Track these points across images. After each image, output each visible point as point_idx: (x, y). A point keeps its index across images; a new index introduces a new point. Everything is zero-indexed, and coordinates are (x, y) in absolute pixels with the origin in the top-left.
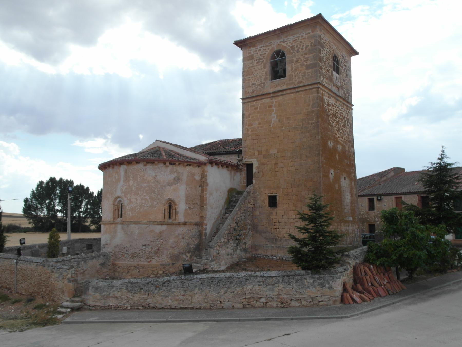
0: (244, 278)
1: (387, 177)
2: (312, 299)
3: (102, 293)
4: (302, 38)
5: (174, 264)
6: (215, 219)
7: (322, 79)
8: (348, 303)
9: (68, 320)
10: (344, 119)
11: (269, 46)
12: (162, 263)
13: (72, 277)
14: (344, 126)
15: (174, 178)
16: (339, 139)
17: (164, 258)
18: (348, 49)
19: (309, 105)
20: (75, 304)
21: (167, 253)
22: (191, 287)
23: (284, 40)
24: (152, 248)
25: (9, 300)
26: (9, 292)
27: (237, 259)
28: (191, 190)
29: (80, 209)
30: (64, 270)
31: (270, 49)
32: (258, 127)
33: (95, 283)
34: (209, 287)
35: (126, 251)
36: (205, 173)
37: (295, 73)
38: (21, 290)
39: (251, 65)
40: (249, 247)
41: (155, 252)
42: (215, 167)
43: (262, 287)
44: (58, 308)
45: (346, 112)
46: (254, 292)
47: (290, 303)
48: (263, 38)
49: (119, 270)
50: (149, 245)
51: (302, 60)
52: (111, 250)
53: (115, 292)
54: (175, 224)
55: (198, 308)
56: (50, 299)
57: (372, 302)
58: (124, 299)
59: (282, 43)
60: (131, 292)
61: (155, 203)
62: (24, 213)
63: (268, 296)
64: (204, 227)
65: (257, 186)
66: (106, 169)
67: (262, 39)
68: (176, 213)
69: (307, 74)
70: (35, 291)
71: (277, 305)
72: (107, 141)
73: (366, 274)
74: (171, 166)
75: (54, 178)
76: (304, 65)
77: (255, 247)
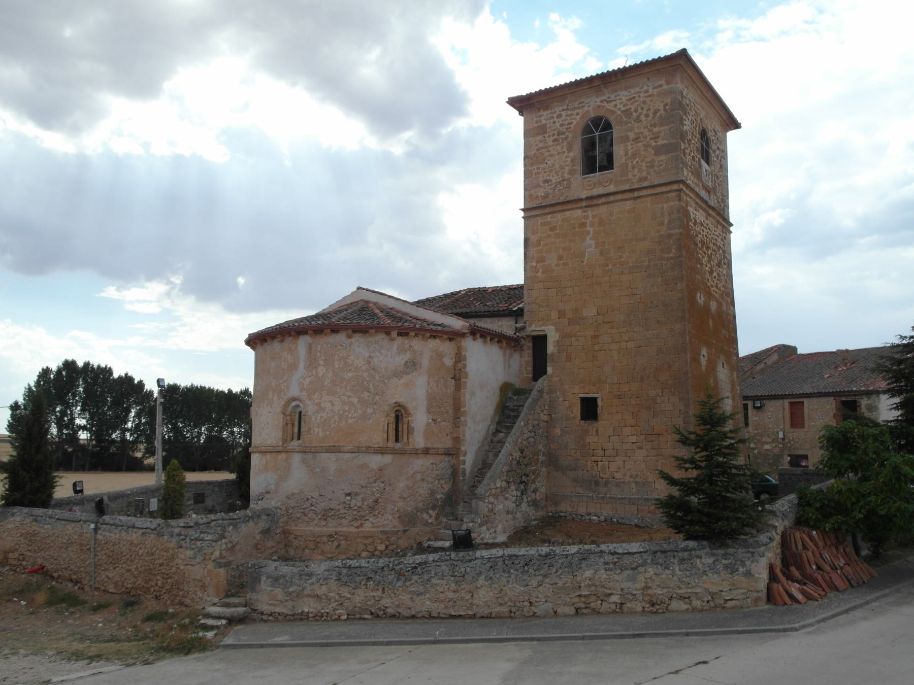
0: (577, 557)
1: (765, 363)
2: (713, 595)
3: (289, 588)
4: (646, 95)
5: (407, 530)
6: (479, 443)
7: (687, 175)
8: (782, 603)
9: (228, 640)
10: (719, 250)
11: (579, 108)
12: (383, 529)
13: (221, 557)
14: (719, 265)
15: (406, 362)
16: (712, 289)
17: (388, 519)
18: (723, 116)
19: (662, 224)
20: (233, 609)
21: (393, 509)
22: (470, 574)
23: (608, 98)
24: (363, 499)
25: (83, 604)
26: (76, 588)
27: (522, 521)
28: (437, 386)
29: (126, 423)
30: (207, 542)
31: (581, 114)
32: (558, 265)
33: (274, 569)
34: (507, 575)
35: (312, 505)
36: (463, 353)
37: (632, 162)
38: (105, 585)
39: (541, 145)
40: (542, 499)
41: (369, 508)
42: (479, 342)
43: (612, 573)
44: (199, 618)
45: (721, 237)
46: (598, 584)
47: (668, 605)
48: (567, 93)
49: (295, 543)
50: (357, 494)
51: (646, 137)
52: (279, 504)
53: (315, 587)
54: (408, 452)
55: (486, 616)
56: (173, 601)
57: (826, 600)
58: (333, 600)
59: (605, 102)
60: (348, 586)
61: (370, 411)
62: (10, 431)
63: (626, 591)
64: (461, 458)
65: (555, 379)
66: (265, 344)
67: (565, 95)
68: (410, 431)
69: (656, 164)
70: (139, 585)
71: (643, 608)
72: (172, 289)
73: (805, 547)
74: (400, 337)
75: (73, 363)
76: (650, 146)
77: (552, 499)
